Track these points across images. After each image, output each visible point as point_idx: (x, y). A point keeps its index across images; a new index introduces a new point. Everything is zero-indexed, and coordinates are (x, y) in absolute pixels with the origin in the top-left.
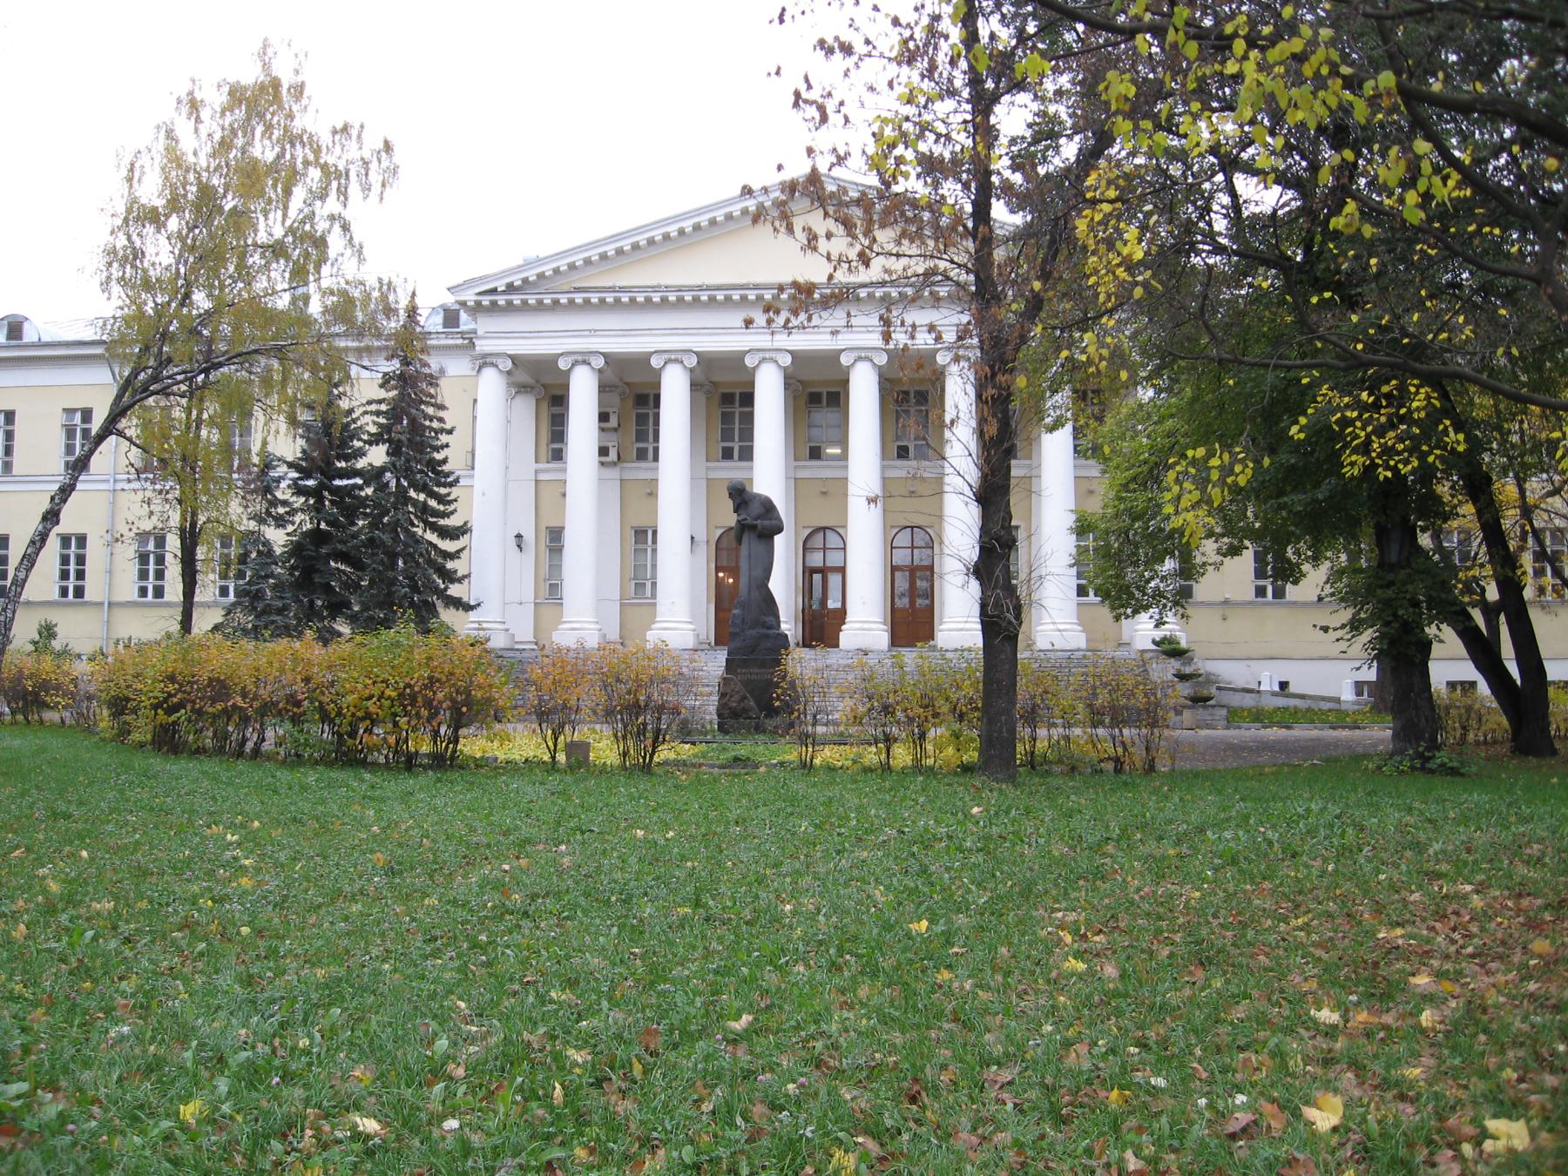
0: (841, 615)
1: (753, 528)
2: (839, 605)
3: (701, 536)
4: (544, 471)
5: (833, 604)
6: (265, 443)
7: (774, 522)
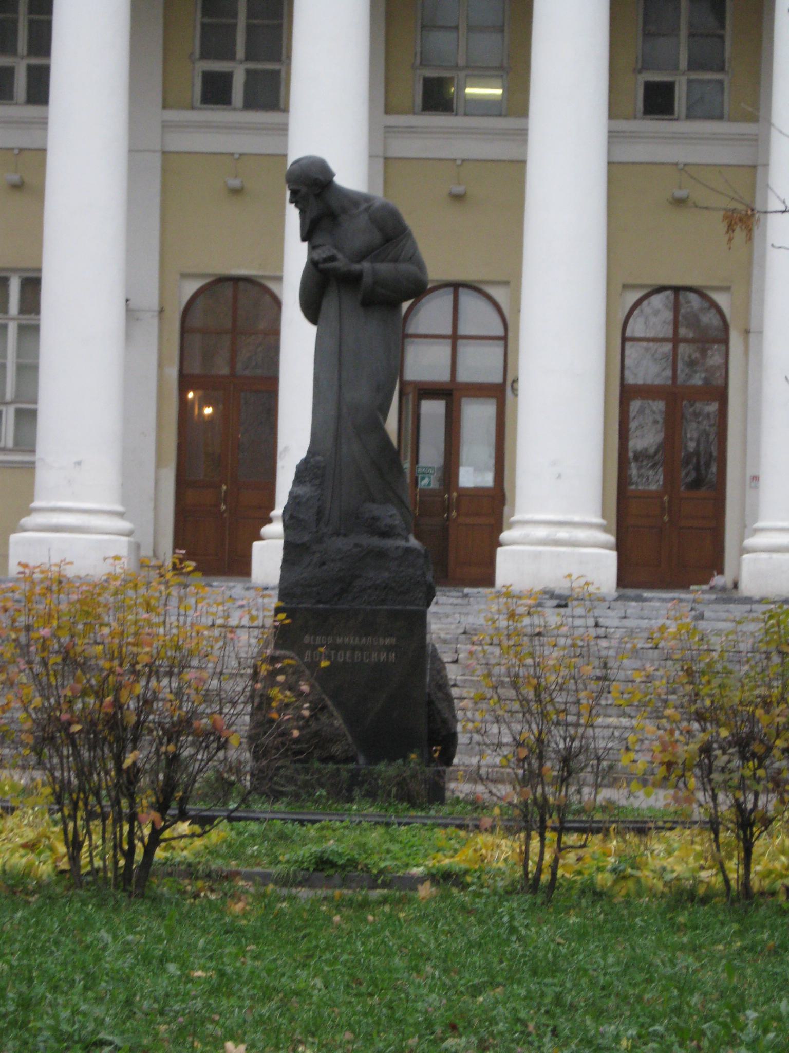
0: (493, 506)
1: (351, 280)
2: (487, 480)
3: (150, 299)
4: (634, 137)
5: (473, 476)
6: (503, 41)
7: (404, 267)
